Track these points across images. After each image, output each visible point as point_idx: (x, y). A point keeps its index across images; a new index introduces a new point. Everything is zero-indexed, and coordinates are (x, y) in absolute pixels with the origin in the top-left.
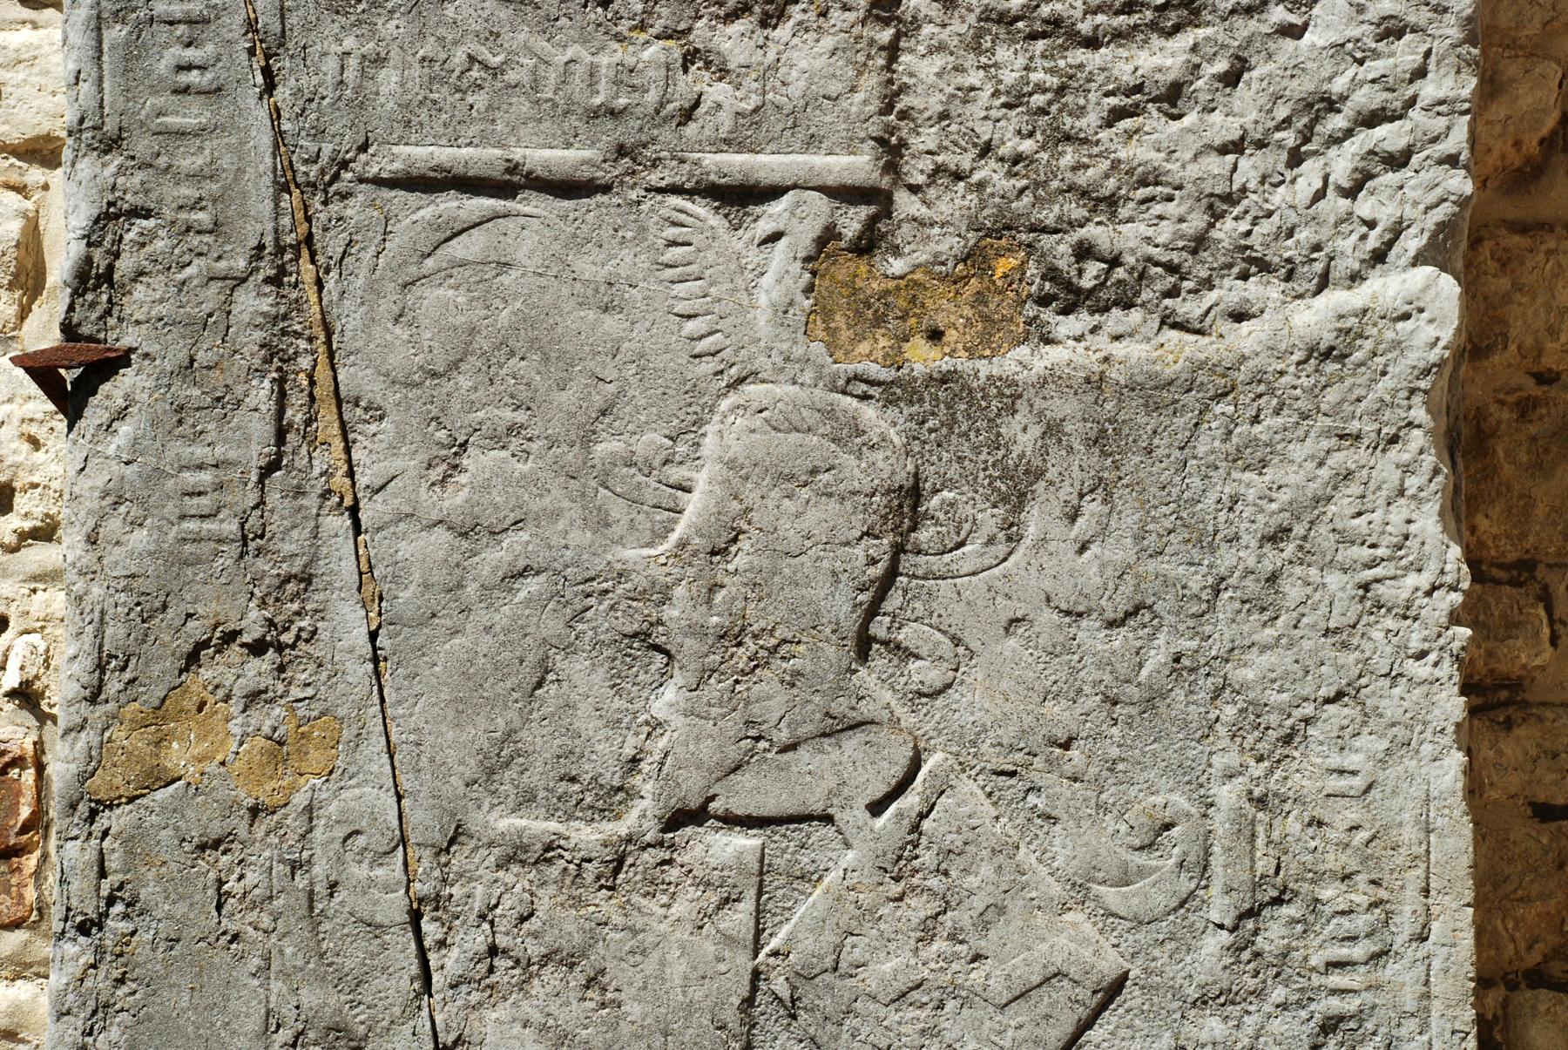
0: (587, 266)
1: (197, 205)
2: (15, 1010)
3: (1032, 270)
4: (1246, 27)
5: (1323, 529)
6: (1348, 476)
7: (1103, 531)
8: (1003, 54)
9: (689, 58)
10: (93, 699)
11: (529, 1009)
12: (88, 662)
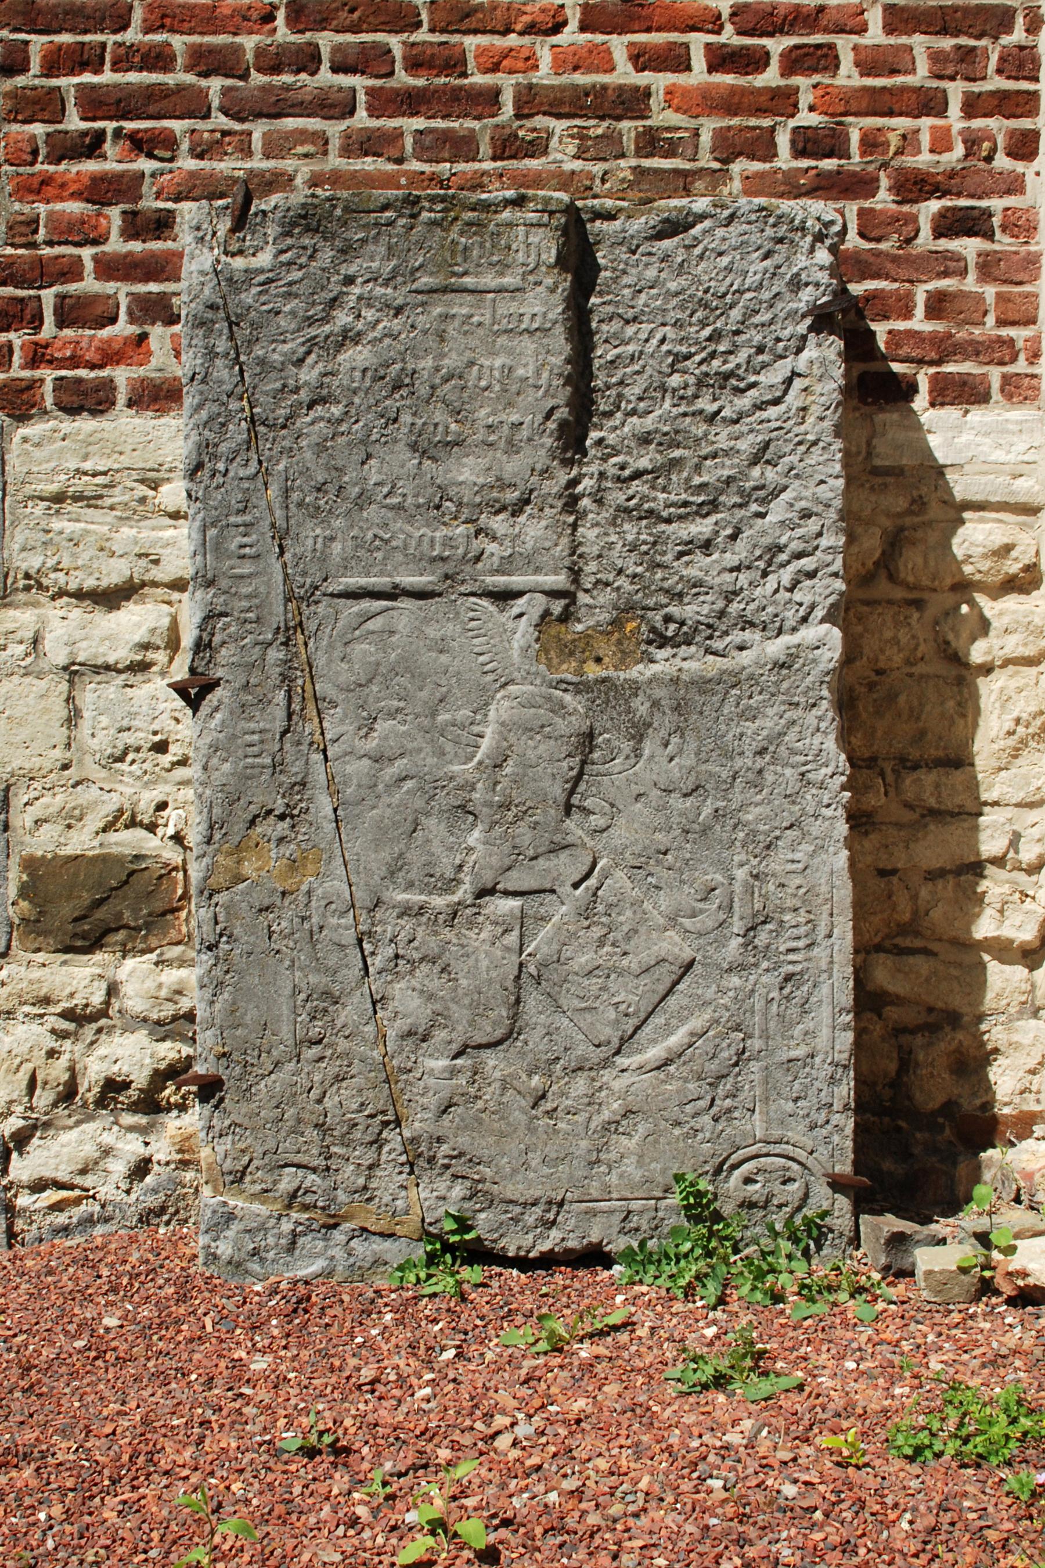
0: (432, 632)
1: (249, 610)
2: (181, 981)
3: (644, 628)
4: (740, 513)
5: (783, 748)
6: (794, 722)
7: (681, 751)
8: (627, 526)
9: (478, 532)
10: (208, 843)
11: (414, 983)
12: (205, 825)
